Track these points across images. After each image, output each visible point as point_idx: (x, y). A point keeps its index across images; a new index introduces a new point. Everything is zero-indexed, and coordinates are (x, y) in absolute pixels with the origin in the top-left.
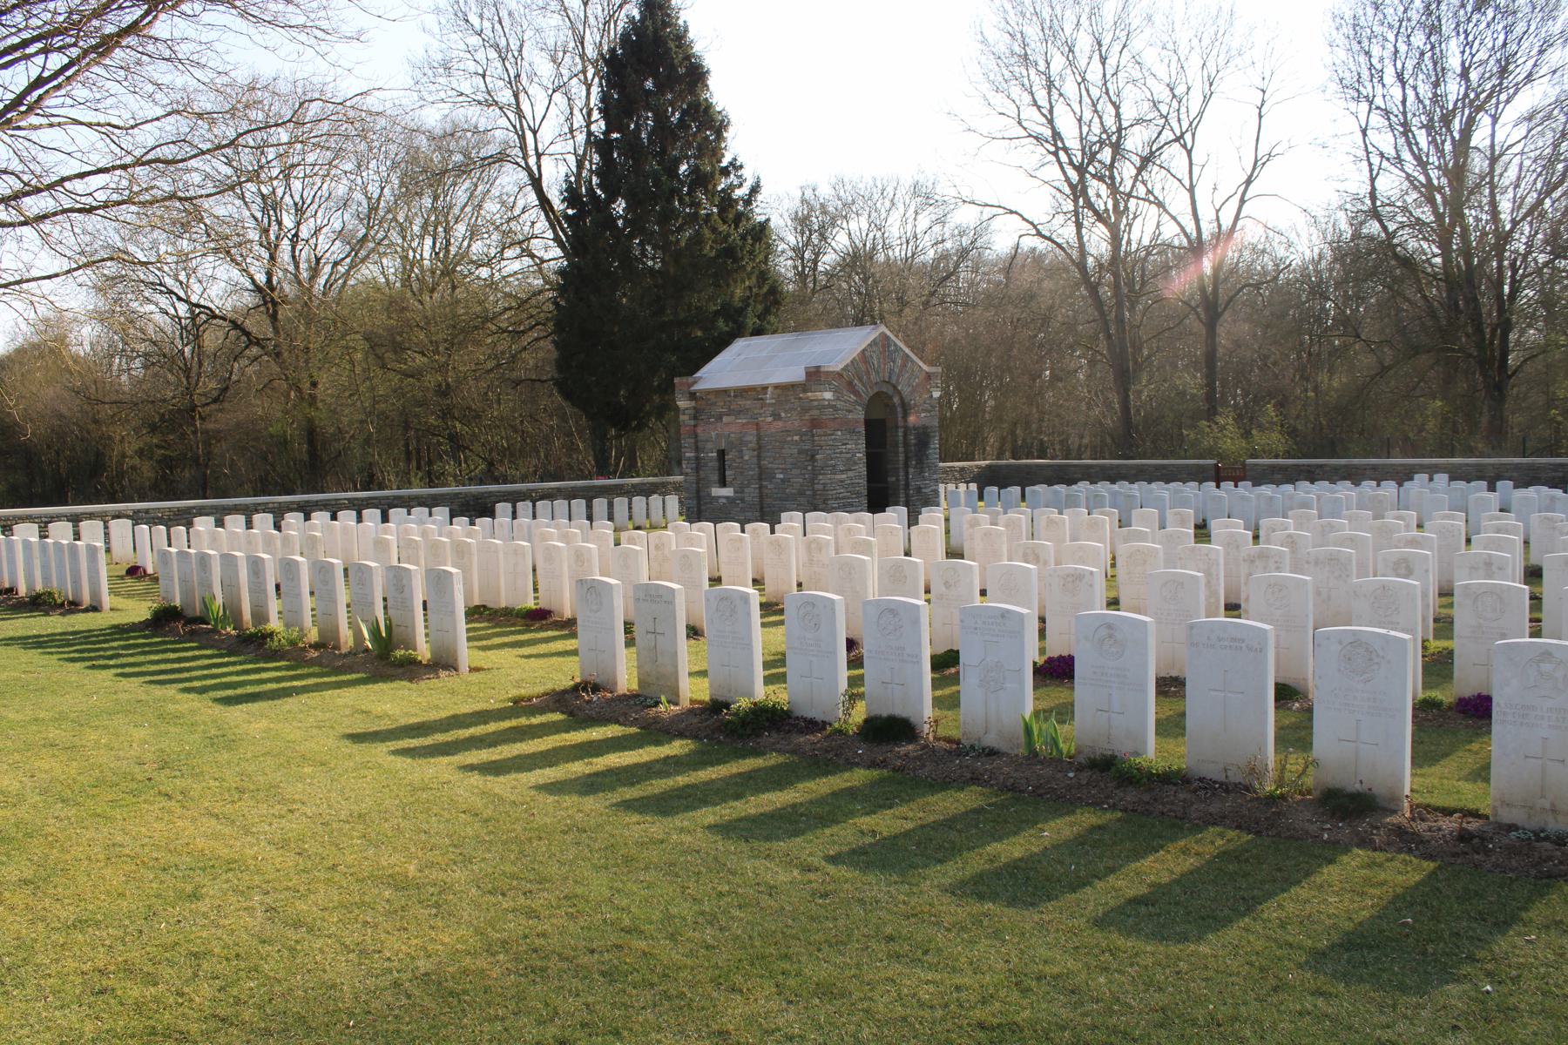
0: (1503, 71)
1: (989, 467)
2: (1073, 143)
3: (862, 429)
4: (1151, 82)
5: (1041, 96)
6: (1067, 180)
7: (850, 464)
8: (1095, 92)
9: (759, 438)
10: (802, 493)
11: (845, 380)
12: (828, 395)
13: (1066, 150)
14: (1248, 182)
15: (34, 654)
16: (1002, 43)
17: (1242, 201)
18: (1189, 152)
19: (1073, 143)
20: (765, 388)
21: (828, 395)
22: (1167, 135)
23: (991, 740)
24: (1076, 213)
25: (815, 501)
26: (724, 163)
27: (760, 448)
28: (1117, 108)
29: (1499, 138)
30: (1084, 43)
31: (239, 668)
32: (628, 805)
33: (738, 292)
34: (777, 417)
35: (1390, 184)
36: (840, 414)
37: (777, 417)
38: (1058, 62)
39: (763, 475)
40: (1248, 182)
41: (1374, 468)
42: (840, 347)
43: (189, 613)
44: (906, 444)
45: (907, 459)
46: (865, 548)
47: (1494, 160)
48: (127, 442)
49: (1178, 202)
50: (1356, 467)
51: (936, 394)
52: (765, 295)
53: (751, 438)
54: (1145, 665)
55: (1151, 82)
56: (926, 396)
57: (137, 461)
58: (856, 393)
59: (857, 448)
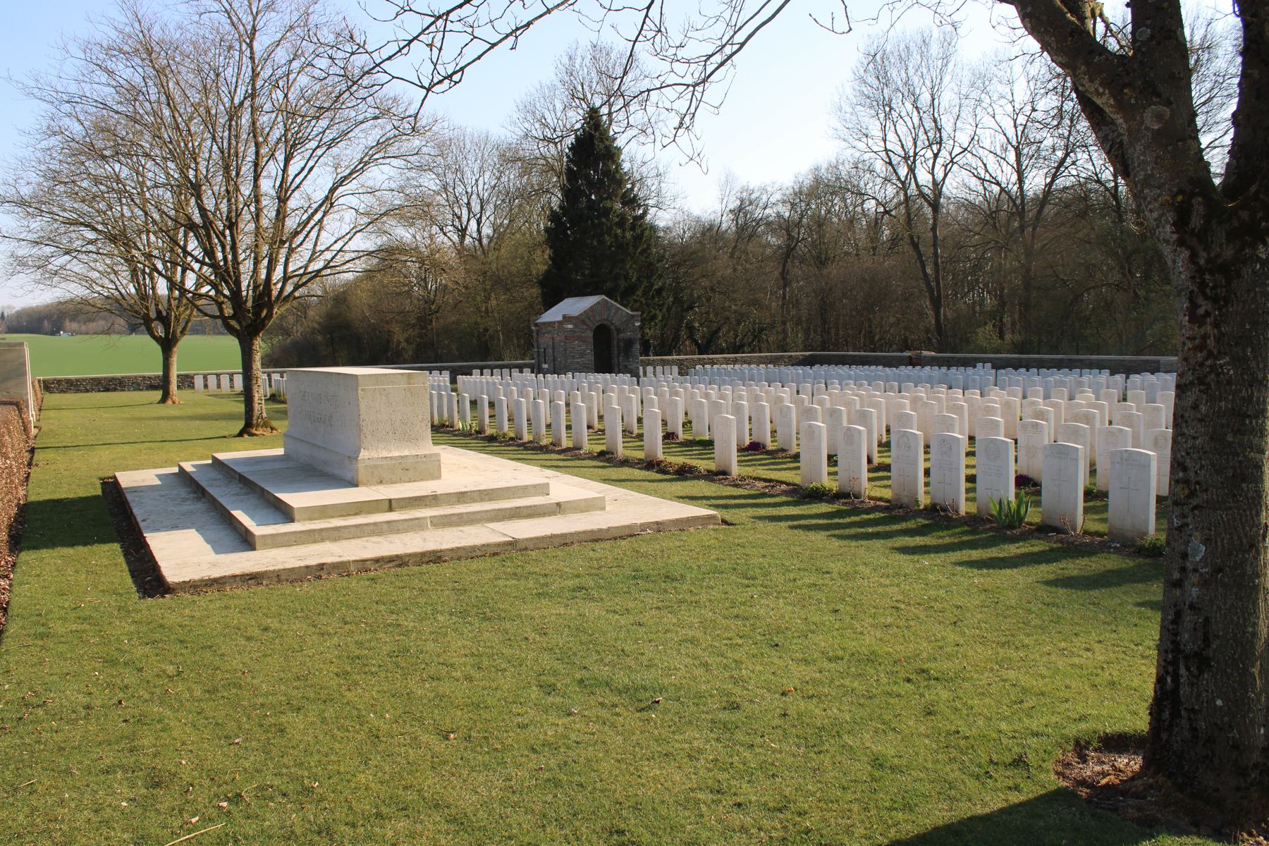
15: (940, 577)
31: (880, 529)
32: (791, 527)
41: (959, 359)
46: (876, 405)
48: (399, 336)
54: (819, 450)
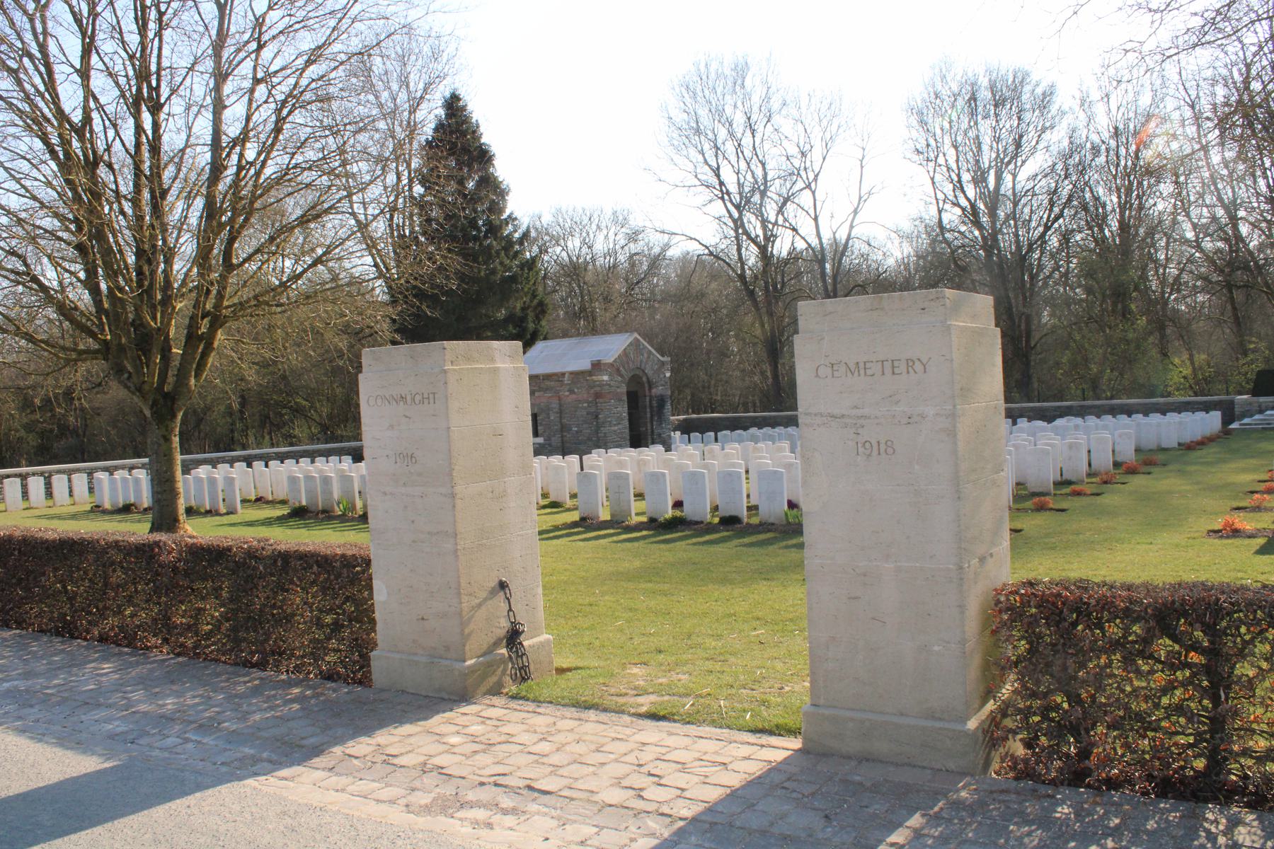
0: (1018, 145)
1: (685, 420)
2: (733, 188)
3: (625, 398)
4: (785, 143)
5: (710, 155)
6: (731, 216)
7: (620, 419)
8: (748, 154)
9: (561, 405)
10: (589, 439)
11: (615, 368)
12: (606, 378)
13: (728, 193)
14: (856, 212)
16: (680, 118)
17: (852, 227)
18: (813, 193)
19: (733, 188)
20: (563, 374)
21: (606, 378)
22: (800, 185)
23: (772, 520)
24: (737, 238)
25: (604, 444)
26: (505, 216)
27: (561, 412)
28: (763, 165)
29: (1018, 187)
30: (739, 120)
33: (519, 305)
34: (572, 392)
35: (952, 216)
36: (613, 389)
37: (572, 392)
38: (722, 133)
39: (564, 428)
40: (856, 212)
42: (611, 347)
43: (313, 509)
44: (651, 407)
45: (652, 416)
47: (1015, 204)
49: (807, 228)
50: (1046, 409)
51: (668, 375)
52: (535, 308)
53: (555, 405)
55: (785, 143)
56: (662, 376)
57: (23, 433)
58: (622, 376)
59: (623, 410)
